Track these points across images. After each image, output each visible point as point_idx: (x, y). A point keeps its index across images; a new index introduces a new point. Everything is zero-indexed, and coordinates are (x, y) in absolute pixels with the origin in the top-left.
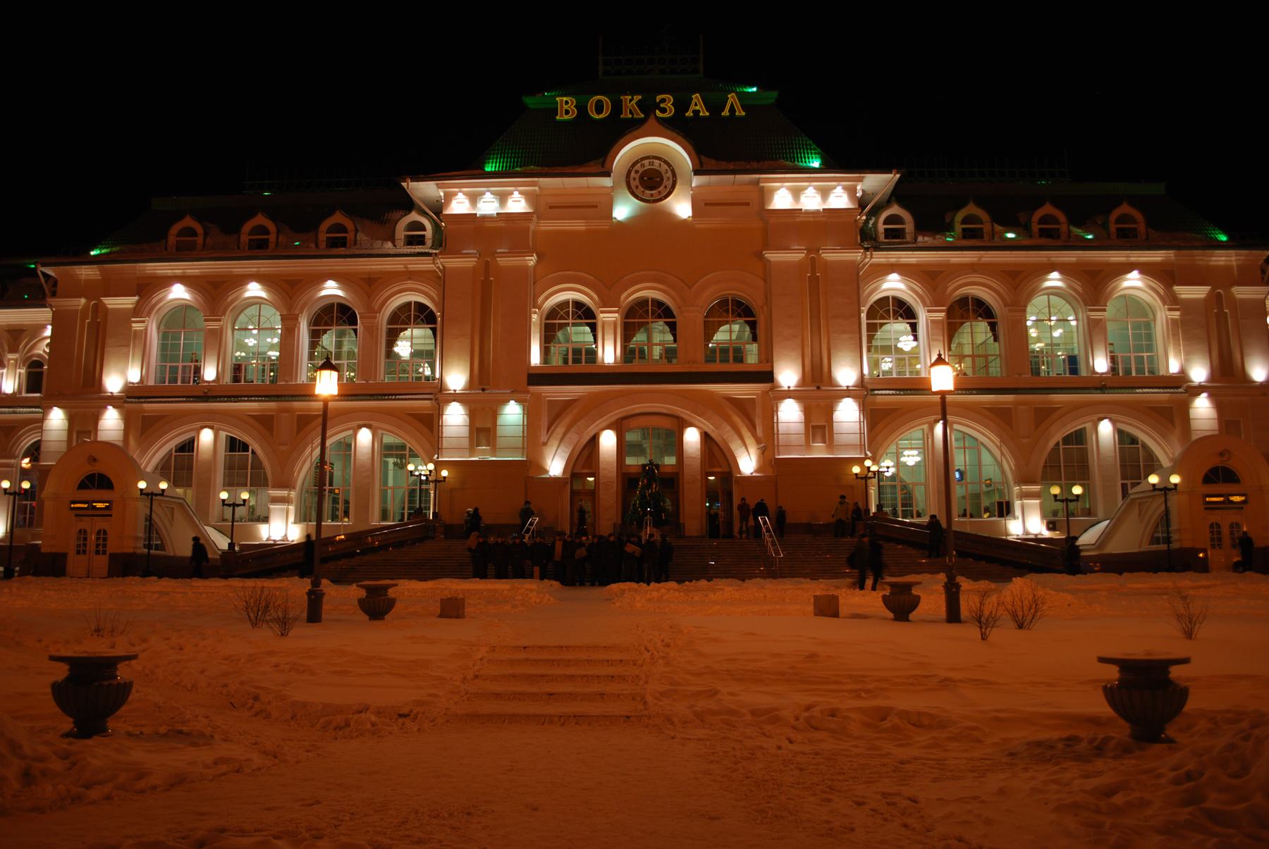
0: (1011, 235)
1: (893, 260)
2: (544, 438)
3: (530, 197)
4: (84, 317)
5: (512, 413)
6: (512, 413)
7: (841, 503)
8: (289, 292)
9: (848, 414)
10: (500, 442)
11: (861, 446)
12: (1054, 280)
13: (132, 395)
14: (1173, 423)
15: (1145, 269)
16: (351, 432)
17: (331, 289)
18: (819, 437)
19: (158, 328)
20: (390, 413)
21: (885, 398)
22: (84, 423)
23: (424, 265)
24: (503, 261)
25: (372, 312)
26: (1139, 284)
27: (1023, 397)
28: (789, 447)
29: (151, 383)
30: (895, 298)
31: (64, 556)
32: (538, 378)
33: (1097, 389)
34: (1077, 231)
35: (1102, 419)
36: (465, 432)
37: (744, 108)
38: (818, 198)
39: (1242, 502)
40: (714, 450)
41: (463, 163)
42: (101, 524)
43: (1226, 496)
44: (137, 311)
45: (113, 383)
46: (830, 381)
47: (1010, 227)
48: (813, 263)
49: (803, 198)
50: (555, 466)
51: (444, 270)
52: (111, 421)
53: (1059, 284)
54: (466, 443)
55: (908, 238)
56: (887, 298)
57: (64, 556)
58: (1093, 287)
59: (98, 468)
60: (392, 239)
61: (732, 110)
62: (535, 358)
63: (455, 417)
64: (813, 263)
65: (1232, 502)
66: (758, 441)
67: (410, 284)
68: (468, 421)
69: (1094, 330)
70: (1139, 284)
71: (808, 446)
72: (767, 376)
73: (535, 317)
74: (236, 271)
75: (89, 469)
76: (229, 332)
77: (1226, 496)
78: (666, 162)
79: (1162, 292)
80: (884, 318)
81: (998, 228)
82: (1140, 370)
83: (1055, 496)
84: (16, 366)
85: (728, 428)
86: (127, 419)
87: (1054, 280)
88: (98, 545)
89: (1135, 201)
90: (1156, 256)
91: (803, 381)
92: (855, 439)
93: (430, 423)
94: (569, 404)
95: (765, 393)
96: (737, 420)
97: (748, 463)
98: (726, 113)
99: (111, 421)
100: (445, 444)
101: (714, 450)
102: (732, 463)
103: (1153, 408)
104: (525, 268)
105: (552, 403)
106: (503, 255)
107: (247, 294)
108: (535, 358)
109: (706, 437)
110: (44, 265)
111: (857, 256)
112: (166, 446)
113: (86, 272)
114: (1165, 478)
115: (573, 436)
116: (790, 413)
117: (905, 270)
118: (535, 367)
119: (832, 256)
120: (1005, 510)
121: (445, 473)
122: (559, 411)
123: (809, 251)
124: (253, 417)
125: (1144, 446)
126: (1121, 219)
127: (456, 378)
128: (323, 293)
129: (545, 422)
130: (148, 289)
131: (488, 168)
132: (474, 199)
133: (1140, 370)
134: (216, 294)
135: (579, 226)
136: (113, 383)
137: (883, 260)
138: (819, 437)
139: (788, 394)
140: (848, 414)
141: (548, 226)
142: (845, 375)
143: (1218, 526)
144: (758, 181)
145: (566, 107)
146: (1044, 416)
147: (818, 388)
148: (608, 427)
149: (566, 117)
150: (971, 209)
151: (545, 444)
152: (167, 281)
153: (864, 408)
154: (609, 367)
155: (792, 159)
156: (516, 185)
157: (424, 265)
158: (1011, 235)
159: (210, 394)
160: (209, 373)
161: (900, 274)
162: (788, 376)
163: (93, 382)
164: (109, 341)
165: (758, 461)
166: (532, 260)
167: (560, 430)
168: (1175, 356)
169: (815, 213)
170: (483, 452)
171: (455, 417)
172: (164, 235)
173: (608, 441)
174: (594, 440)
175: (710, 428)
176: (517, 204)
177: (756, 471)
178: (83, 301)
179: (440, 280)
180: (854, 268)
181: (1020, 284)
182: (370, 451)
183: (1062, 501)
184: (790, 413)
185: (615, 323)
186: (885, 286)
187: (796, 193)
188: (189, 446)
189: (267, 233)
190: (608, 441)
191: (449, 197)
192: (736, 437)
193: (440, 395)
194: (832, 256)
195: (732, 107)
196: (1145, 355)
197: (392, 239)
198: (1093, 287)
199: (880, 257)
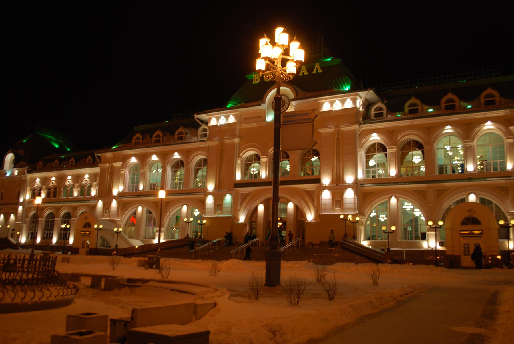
0: (431, 110)
1: (374, 127)
2: (239, 208)
3: (236, 116)
4: (108, 170)
5: (228, 198)
6: (228, 198)
7: (331, 233)
8: (164, 157)
9: (349, 195)
10: (224, 210)
11: (354, 209)
12: (448, 129)
13: (121, 195)
14: (508, 194)
15: (493, 120)
16: (180, 207)
17: (177, 156)
18: (338, 205)
19: (130, 172)
20: (192, 199)
21: (368, 187)
22: (107, 206)
23: (202, 145)
24: (227, 142)
25: (189, 163)
26: (492, 127)
27: (433, 186)
28: (325, 210)
29: (127, 191)
30: (378, 143)
31: (78, 248)
32: (239, 185)
33: (467, 179)
34: (463, 104)
35: (470, 194)
36: (330, 202)
37: (322, 68)
38: (340, 105)
39: (480, 234)
40: (299, 212)
41: (219, 105)
42: (476, 241)
43: (85, 232)
44: (122, 167)
45: (115, 192)
46: (343, 181)
47: (431, 106)
48: (338, 132)
49: (334, 105)
50: (242, 219)
51: (208, 147)
52: (114, 204)
53: (451, 131)
54: (213, 210)
55: (385, 116)
56: (374, 144)
57: (78, 248)
58: (467, 131)
59: (88, 221)
60: (197, 136)
61: (317, 70)
62: (238, 176)
63: (210, 200)
64: (338, 132)
65: (474, 233)
66: (315, 207)
67: (200, 152)
68: (214, 203)
69: (469, 152)
70: (492, 127)
71: (333, 209)
72: (318, 181)
73: (239, 162)
74: (149, 151)
75: (467, 215)
76: (148, 173)
77: (85, 232)
78: (286, 96)
79: (504, 130)
80: (373, 152)
81: (425, 107)
82: (495, 169)
83: (384, 231)
84: (78, 188)
85: (303, 202)
86: (118, 203)
87: (448, 129)
88: (465, 251)
89: (494, 86)
90: (500, 113)
91: (332, 182)
92: (352, 206)
93: (202, 203)
94: (248, 194)
95: (318, 187)
96: (307, 199)
97: (310, 217)
98: (314, 72)
99: (114, 204)
100: (206, 211)
101: (299, 212)
102: (304, 216)
103: (199, 200)
104: (234, 144)
105: (242, 194)
106: (227, 139)
107: (152, 159)
108: (238, 176)
109: (296, 207)
110: (97, 153)
111: (356, 127)
112: (128, 214)
113: (109, 155)
114: (98, 226)
115: (248, 207)
116: (326, 195)
117: (379, 131)
118: (239, 181)
119: (345, 128)
120: (424, 237)
121: (204, 221)
122: (245, 197)
123: (336, 127)
124: (153, 202)
125: (496, 205)
126: (487, 96)
127: (211, 187)
128: (485, 128)
129: (239, 202)
130: (125, 159)
131: (228, 106)
132: (332, 104)
133: (495, 169)
134: (143, 159)
135: (254, 125)
136: (115, 192)
137: (369, 128)
138: (338, 205)
139: (326, 188)
140: (349, 195)
141: (244, 126)
142: (349, 179)
143: (468, 245)
144: (316, 101)
145: (256, 78)
146: (441, 193)
147: (337, 185)
148: (261, 203)
149: (256, 82)
150: (413, 100)
151: (239, 210)
152: (130, 156)
153: (356, 193)
154: (263, 179)
155: (339, 88)
156: (213, 115)
157: (202, 145)
158: (431, 110)
159: (471, 177)
160: (141, 187)
161: (377, 133)
162: (326, 180)
163: (110, 191)
164: (114, 178)
165: (315, 215)
166: (237, 140)
167: (244, 205)
168: (510, 161)
169: (339, 111)
170: (219, 214)
171: (210, 200)
172: (131, 141)
173: (261, 208)
174: (256, 209)
175: (297, 203)
176: (232, 120)
177: (313, 220)
178: (108, 164)
179: (207, 150)
180: (354, 132)
181: (433, 132)
182: (396, 207)
183: (387, 233)
184: (326, 195)
185: (266, 162)
186: (371, 139)
187: (332, 104)
188: (135, 213)
189: (454, 101)
190: (261, 208)
191: (210, 119)
192: (306, 206)
193: (206, 193)
194: (345, 128)
195: (317, 69)
196: (499, 161)
197: (197, 136)
198: (467, 131)
199: (366, 127)
